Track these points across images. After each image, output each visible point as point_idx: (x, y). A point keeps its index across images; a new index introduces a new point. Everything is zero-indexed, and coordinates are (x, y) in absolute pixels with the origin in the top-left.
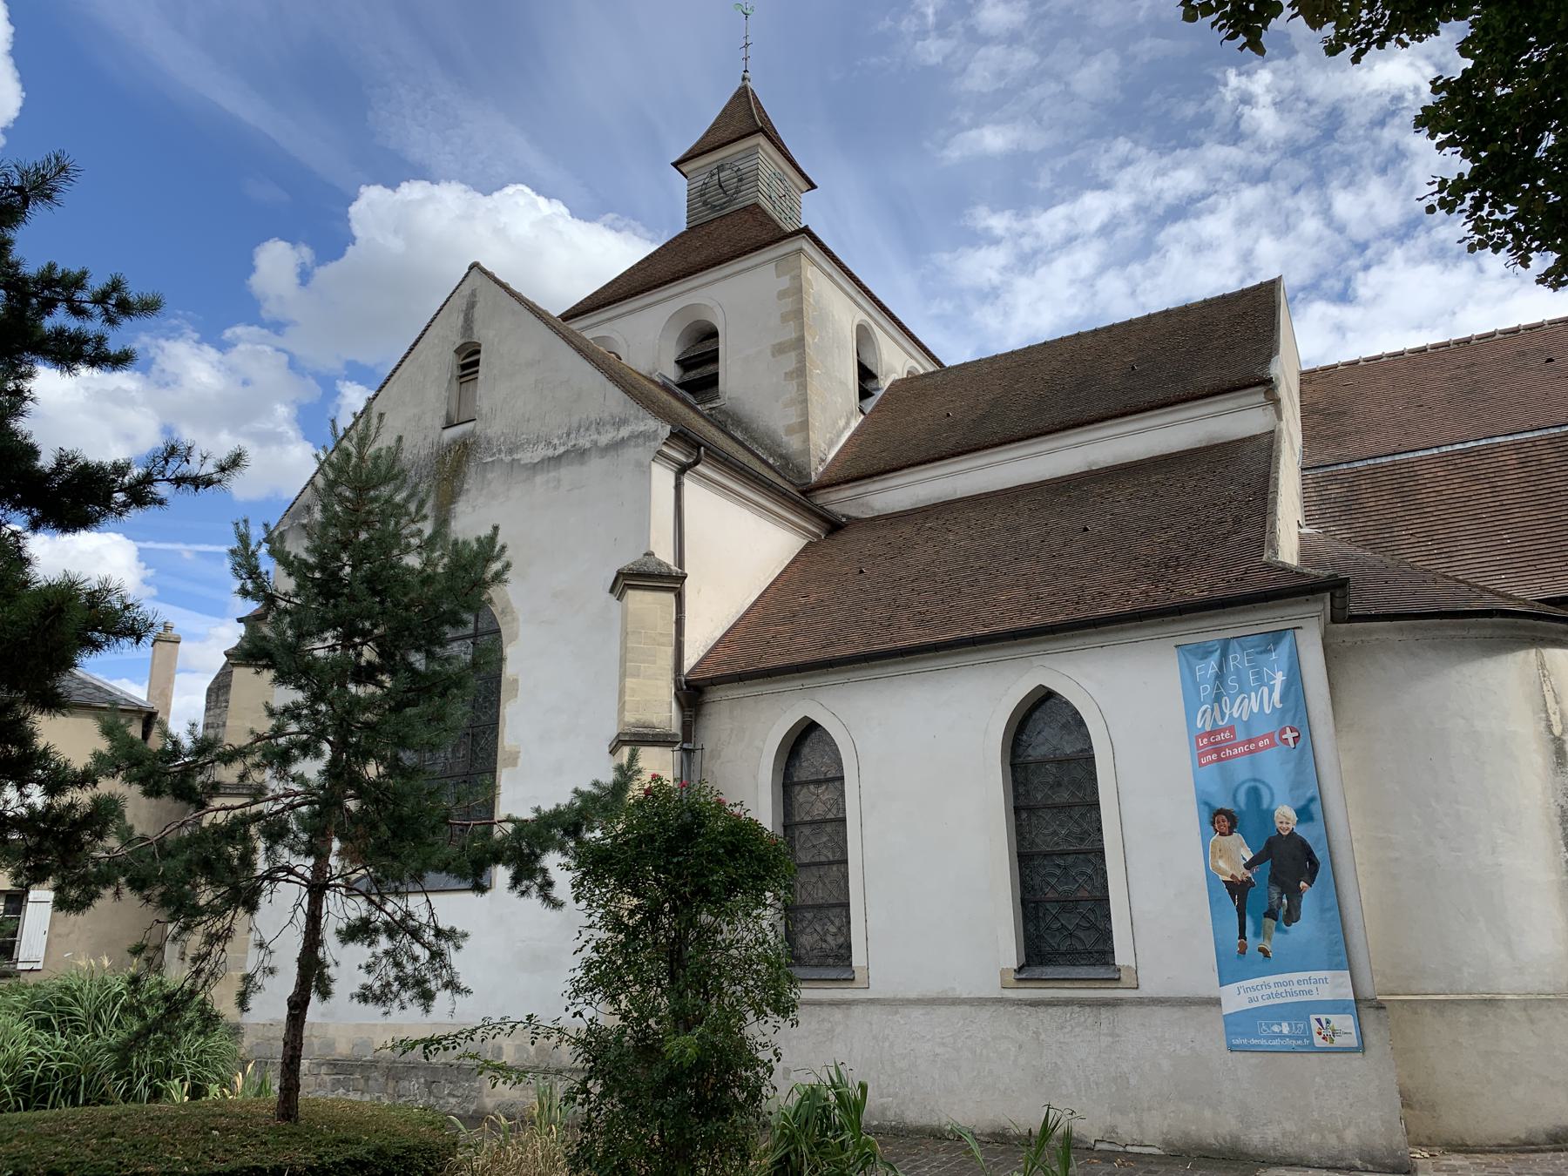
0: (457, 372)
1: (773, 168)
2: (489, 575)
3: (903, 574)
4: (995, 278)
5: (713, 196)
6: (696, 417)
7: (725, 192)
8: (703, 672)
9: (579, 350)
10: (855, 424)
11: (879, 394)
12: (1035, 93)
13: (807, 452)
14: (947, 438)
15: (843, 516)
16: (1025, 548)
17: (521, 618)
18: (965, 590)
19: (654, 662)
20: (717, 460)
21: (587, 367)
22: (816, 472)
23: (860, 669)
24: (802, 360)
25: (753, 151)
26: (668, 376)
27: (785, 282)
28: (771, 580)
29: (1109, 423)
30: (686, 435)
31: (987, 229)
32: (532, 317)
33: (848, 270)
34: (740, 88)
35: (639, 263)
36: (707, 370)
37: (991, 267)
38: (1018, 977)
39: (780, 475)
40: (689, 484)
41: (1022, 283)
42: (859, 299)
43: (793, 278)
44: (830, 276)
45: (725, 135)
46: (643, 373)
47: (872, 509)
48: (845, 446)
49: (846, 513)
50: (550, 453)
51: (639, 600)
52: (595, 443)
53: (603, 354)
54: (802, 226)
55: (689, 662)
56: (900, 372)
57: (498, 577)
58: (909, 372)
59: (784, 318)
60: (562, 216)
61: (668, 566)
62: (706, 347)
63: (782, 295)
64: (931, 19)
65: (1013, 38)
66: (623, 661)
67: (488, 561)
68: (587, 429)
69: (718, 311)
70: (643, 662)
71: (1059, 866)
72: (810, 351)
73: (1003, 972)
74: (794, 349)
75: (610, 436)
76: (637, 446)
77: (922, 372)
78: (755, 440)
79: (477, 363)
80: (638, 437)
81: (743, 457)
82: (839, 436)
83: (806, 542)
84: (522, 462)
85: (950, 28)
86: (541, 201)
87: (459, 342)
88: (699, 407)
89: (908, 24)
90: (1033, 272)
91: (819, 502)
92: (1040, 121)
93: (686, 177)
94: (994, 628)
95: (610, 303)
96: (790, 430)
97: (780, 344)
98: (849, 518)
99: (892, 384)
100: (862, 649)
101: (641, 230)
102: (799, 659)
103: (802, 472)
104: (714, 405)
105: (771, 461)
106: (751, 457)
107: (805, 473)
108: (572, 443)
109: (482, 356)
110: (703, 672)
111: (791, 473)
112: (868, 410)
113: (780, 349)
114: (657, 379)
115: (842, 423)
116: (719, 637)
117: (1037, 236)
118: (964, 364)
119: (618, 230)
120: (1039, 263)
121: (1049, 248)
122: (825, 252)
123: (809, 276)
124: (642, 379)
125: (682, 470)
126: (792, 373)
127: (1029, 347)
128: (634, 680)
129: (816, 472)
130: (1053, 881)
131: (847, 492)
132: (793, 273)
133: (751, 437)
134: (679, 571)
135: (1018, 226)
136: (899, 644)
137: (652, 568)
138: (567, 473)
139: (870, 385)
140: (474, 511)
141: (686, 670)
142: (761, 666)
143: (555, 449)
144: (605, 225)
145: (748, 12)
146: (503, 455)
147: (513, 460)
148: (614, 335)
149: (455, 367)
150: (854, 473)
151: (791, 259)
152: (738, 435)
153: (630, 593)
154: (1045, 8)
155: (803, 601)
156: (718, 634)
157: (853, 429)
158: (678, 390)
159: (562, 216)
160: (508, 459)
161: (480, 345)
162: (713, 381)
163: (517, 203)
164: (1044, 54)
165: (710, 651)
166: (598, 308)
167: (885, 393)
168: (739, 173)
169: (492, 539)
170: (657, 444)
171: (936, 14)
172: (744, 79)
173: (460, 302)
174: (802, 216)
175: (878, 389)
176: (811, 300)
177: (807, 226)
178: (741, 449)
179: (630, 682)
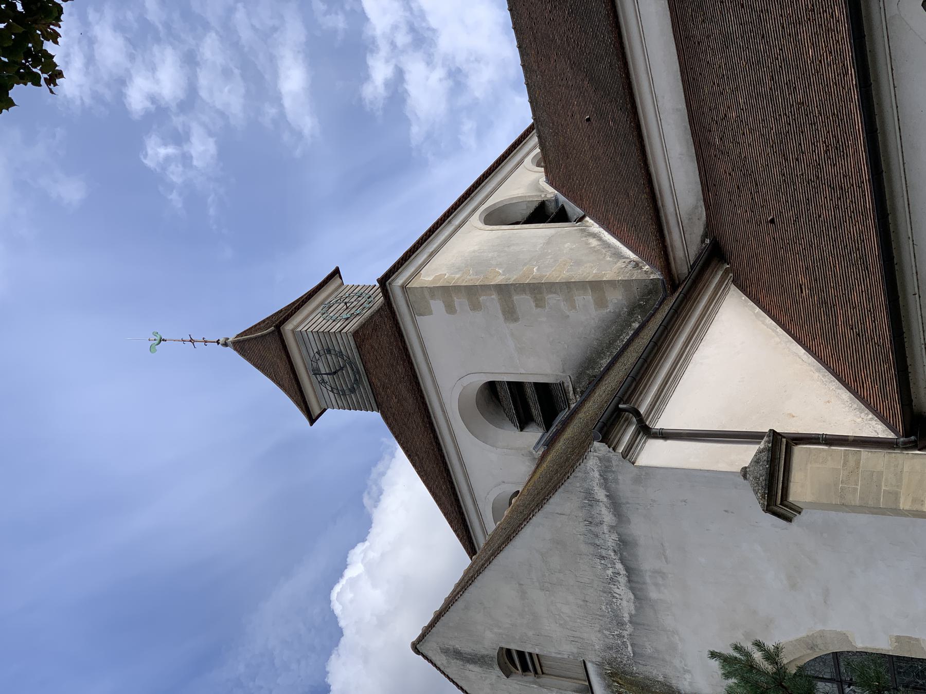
0: (531, 676)
2: (768, 667)
3: (776, 171)
4: (439, 73)
5: (345, 381)
6: (585, 409)
7: (341, 369)
9: (508, 539)
10: (595, 228)
11: (562, 199)
12: (246, 35)
13: (626, 284)
14: (614, 120)
15: (703, 241)
16: (749, 26)
17: (819, 627)
18: (800, 97)
20: (635, 389)
21: (527, 533)
22: (650, 273)
23: (896, 225)
24: (521, 288)
25: (300, 337)
26: (537, 440)
27: (437, 305)
28: (779, 330)
29: (633, 76)
30: (605, 424)
31: (387, 84)
32: (471, 589)
33: (422, 237)
34: (235, 349)
35: (414, 465)
37: (427, 78)
39: (653, 315)
40: (664, 422)
41: (444, 43)
42: (457, 222)
43: (433, 297)
44: (432, 255)
45: (282, 367)
46: (533, 467)
47: (696, 207)
49: (699, 239)
50: (622, 580)
52: (612, 528)
53: (512, 511)
54: (378, 285)
55: (877, 429)
56: (537, 175)
57: (772, 656)
58: (538, 165)
59: (476, 306)
60: (365, 552)
61: (760, 452)
62: (505, 395)
63: (450, 309)
64: (170, 150)
65: (190, 60)
66: (877, 511)
67: (752, 666)
68: (597, 536)
69: (466, 381)
70: (879, 486)
72: (513, 278)
75: (604, 511)
76: (616, 481)
77: (538, 150)
78: (611, 344)
79: (521, 654)
80: (606, 480)
81: (631, 357)
82: (608, 245)
83: (733, 287)
84: (633, 612)
85: (180, 129)
86: (350, 573)
87: (497, 671)
88: (573, 406)
89: (176, 175)
90: (434, 31)
91: (684, 270)
92: (275, 29)
93: (325, 410)
94: (848, 62)
95: (457, 500)
96: (601, 303)
97: (504, 312)
98: (705, 236)
99: (551, 184)
100: (870, 222)
101: (380, 467)
102: (881, 298)
103: (650, 290)
104: (571, 389)
105: (636, 325)
106: (631, 348)
107: (651, 286)
108: (612, 554)
109: (514, 647)
110: (894, 415)
111: (651, 302)
112: (579, 212)
113: (510, 314)
114: (540, 453)
115: (594, 242)
116: (849, 394)
117: (395, 27)
118: (531, 102)
119: (381, 492)
120: (424, 24)
121: (408, 14)
122: (406, 261)
123: (430, 278)
124: (541, 470)
125: (646, 431)
126: (536, 300)
127: (514, 28)
128: (902, 500)
129: (650, 273)
131: (675, 237)
133: (608, 348)
134: (766, 439)
135: (384, 49)
136: (866, 176)
137: (762, 471)
138: (647, 563)
139: (552, 209)
140: (689, 672)
141: (891, 435)
142: (888, 345)
143: (619, 574)
144: (376, 507)
145: (158, 338)
146: (625, 633)
147: (631, 622)
148: (492, 498)
149: (525, 678)
150: (652, 228)
152: (605, 362)
153: (792, 498)
154: (160, 27)
155: (806, 292)
156: (846, 395)
157: (601, 230)
158: (553, 429)
159: (365, 552)
160: (629, 628)
161: (501, 649)
162: (543, 389)
163: (351, 601)
164: (207, 26)
165: (868, 405)
166: (462, 514)
167: (561, 193)
168: (322, 352)
169: (726, 660)
170: (615, 457)
171: (165, 145)
172: (225, 345)
173: (454, 667)
174: (367, 284)
175: (557, 200)
176: (458, 276)
177: (378, 280)
178: (621, 360)
179: (905, 504)
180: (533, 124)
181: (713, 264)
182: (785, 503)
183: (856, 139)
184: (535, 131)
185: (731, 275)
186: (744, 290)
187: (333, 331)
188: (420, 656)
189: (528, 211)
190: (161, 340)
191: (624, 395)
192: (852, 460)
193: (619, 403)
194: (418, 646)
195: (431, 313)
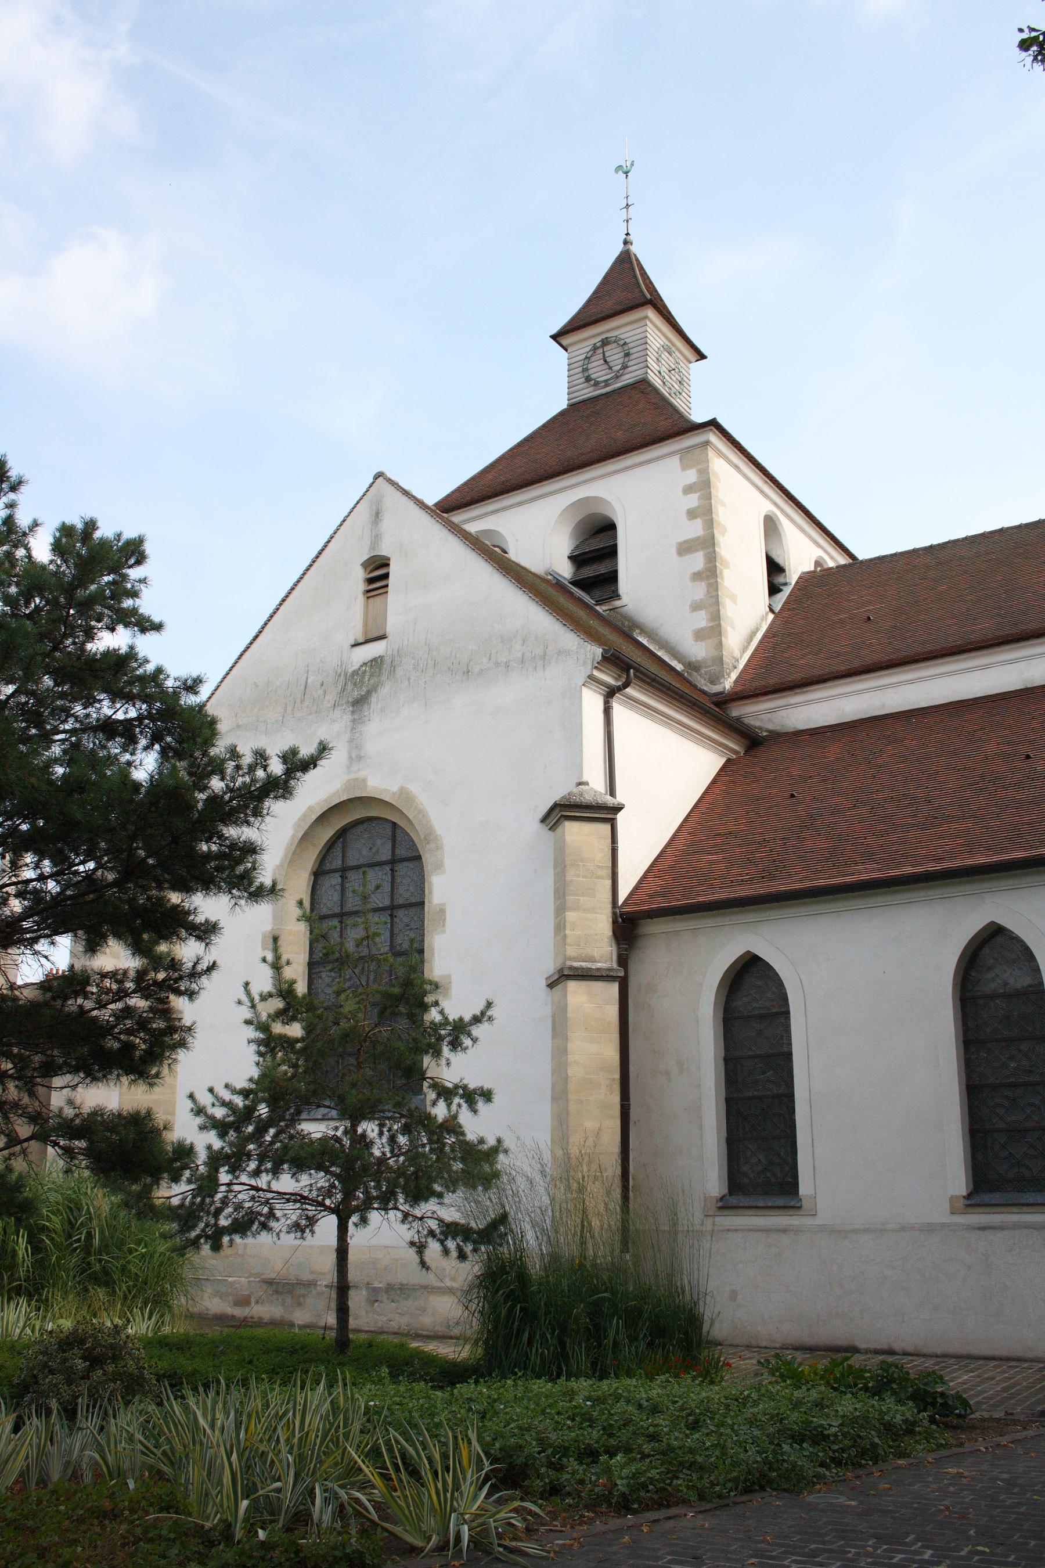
1: (663, 341)
7: (610, 368)
8: (636, 904)
11: (787, 591)
19: (594, 896)
24: (712, 558)
27: (691, 476)
30: (618, 658)
34: (622, 253)
36: (601, 569)
38: (969, 1202)
40: (618, 710)
44: (736, 467)
45: (608, 306)
48: (756, 650)
51: (575, 832)
63: (688, 490)
70: (583, 895)
71: (1007, 1098)
73: (952, 1199)
74: (702, 549)
79: (386, 576)
88: (598, 608)
96: (700, 635)
99: (800, 578)
112: (777, 609)
113: (685, 548)
125: (610, 693)
130: (1001, 1111)
132: (700, 467)
139: (780, 579)
151: (697, 451)
158: (574, 590)
161: (389, 559)
162: (612, 578)
168: (626, 348)
172: (626, 242)
175: (785, 584)
179: (570, 916)
180: (857, 559)
181: (743, 740)
182: (563, 819)
183: (879, 870)
184: (851, 561)
185: (734, 757)
186: (723, 769)
187: (649, 359)
188: (372, 480)
189: (779, 560)
190: (626, 173)
191: (642, 673)
192: (600, 873)
193: (634, 669)
194: (381, 478)
195: (683, 469)
